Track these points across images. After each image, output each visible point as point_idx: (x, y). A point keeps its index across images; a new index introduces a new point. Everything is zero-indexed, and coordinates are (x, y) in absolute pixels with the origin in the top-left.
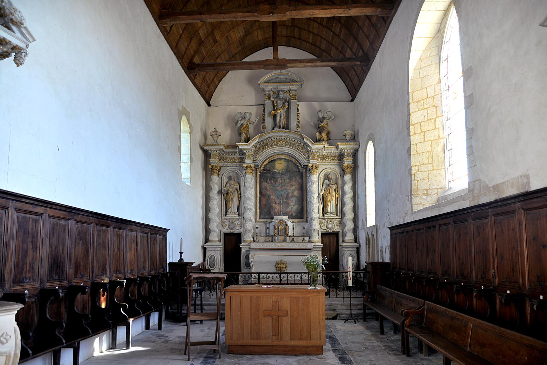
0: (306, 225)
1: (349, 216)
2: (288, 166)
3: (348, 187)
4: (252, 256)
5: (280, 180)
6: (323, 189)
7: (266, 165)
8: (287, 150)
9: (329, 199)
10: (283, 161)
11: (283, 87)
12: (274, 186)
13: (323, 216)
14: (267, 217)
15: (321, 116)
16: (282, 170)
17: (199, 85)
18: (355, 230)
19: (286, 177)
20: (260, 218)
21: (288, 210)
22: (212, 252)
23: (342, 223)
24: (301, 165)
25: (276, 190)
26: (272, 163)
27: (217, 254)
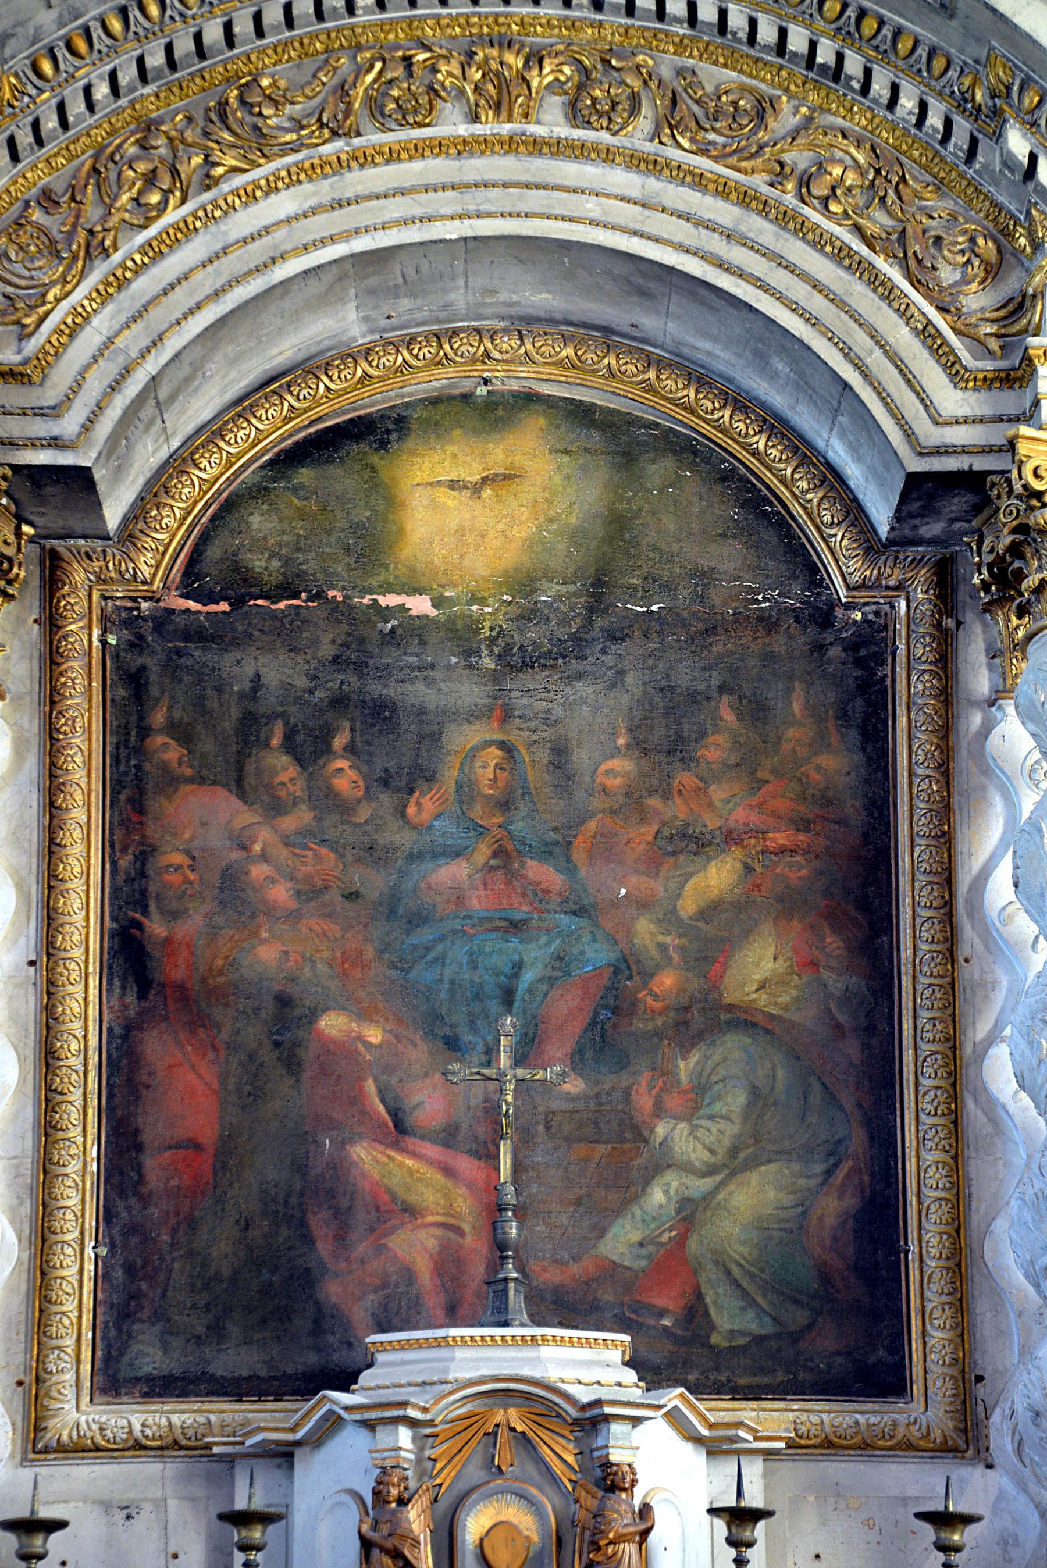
2: (618, 526)
5: (472, 751)
7: (229, 508)
8: (612, 200)
12: (373, 853)
14: (235, 1359)
16: (523, 584)
19: (594, 716)
20: (112, 1381)
21: (622, 1241)
25: (402, 913)
26: (340, 478)
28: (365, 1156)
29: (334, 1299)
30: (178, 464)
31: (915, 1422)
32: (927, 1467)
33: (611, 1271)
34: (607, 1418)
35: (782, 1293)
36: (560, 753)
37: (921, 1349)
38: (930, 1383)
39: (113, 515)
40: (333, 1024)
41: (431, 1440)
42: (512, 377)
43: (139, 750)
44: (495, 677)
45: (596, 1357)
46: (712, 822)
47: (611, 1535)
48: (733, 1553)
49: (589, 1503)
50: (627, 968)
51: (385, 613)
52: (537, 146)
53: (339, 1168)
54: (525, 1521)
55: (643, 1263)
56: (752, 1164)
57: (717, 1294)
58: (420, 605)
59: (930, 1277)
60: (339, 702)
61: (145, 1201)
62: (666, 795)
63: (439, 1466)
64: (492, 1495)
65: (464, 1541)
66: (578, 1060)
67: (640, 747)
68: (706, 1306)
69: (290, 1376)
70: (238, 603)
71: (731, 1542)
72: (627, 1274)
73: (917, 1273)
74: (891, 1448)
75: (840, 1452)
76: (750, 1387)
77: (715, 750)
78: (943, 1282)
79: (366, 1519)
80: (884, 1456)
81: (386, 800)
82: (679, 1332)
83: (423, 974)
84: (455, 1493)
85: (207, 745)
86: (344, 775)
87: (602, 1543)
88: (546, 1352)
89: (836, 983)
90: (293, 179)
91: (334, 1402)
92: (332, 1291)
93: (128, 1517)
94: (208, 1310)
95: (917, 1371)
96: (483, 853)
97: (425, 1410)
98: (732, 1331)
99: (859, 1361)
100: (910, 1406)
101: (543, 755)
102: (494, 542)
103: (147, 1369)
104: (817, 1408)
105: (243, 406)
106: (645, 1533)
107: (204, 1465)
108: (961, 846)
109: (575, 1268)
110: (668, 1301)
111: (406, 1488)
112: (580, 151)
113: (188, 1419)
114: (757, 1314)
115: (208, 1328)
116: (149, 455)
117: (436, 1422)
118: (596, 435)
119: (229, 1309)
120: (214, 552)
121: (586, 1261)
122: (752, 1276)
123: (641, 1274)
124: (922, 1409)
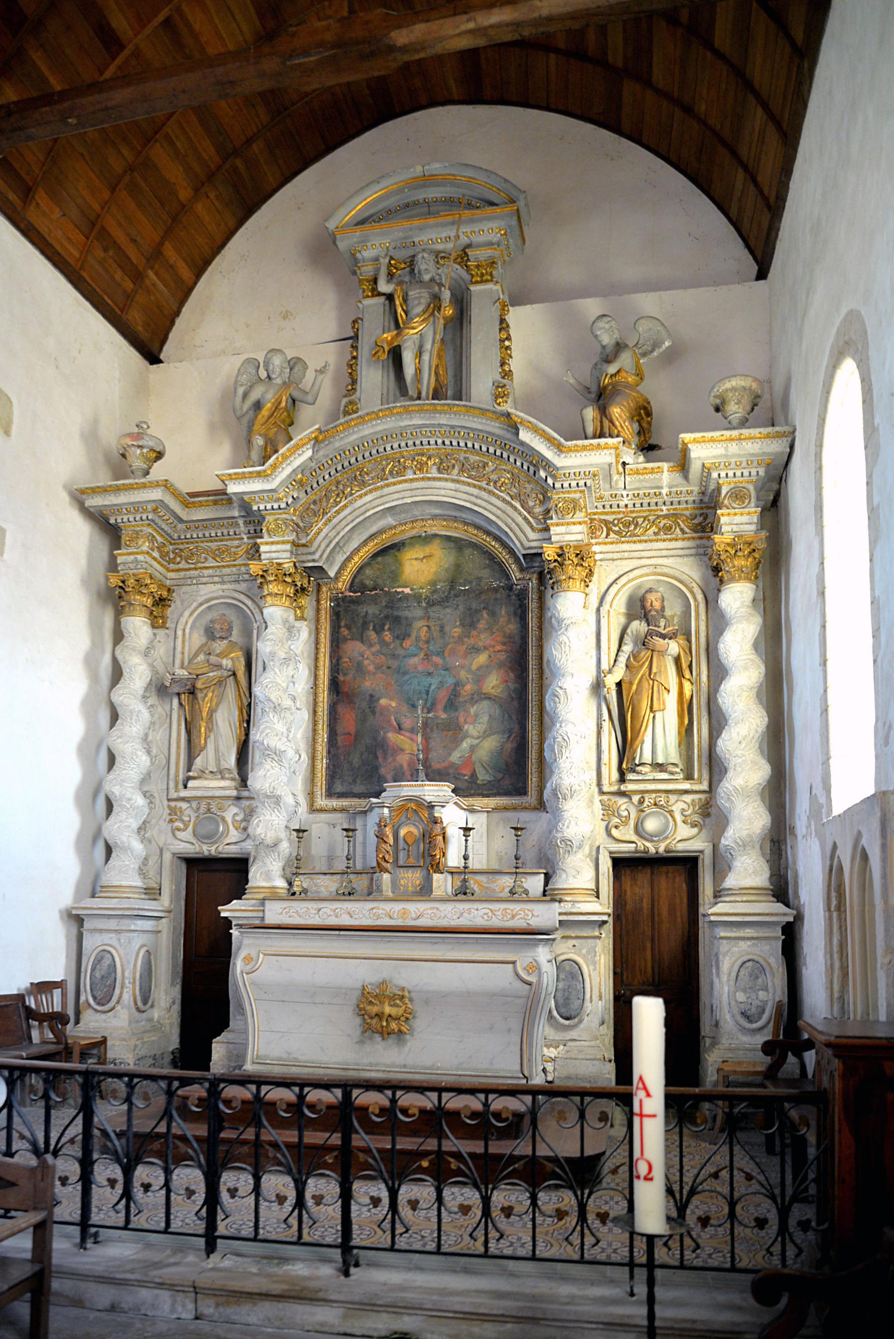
0: (536, 823)
1: (746, 771)
2: (458, 566)
3: (739, 643)
4: (248, 959)
5: (420, 628)
6: (623, 659)
7: (361, 569)
8: (449, 490)
9: (645, 704)
10: (435, 549)
11: (437, 235)
13: (622, 779)
14: (358, 788)
15: (607, 339)
16: (433, 583)
17: (72, 253)
18: (778, 843)
19: (451, 617)
20: (330, 794)
22: (107, 938)
23: (710, 813)
24: (512, 552)
25: (401, 672)
26: (388, 559)
27: (143, 942)
28: (392, 736)
30: (349, 559)
33: (452, 765)
36: (442, 627)
39: (332, 574)
40: (383, 702)
42: (435, 530)
43: (338, 632)
44: (426, 608)
46: (481, 644)
50: (457, 684)
51: (399, 593)
52: (429, 479)
53: (384, 739)
56: (489, 736)
58: (407, 590)
60: (387, 617)
61: (338, 748)
62: (469, 637)
66: (445, 709)
67: (462, 625)
70: (362, 593)
77: (482, 625)
81: (397, 642)
83: (406, 688)
85: (354, 630)
86: (387, 636)
89: (512, 686)
90: (371, 491)
92: (383, 771)
96: (422, 655)
101: (438, 628)
102: (426, 572)
105: (365, 543)
108: (545, 648)
112: (440, 479)
116: (340, 559)
118: (452, 544)
120: (357, 580)
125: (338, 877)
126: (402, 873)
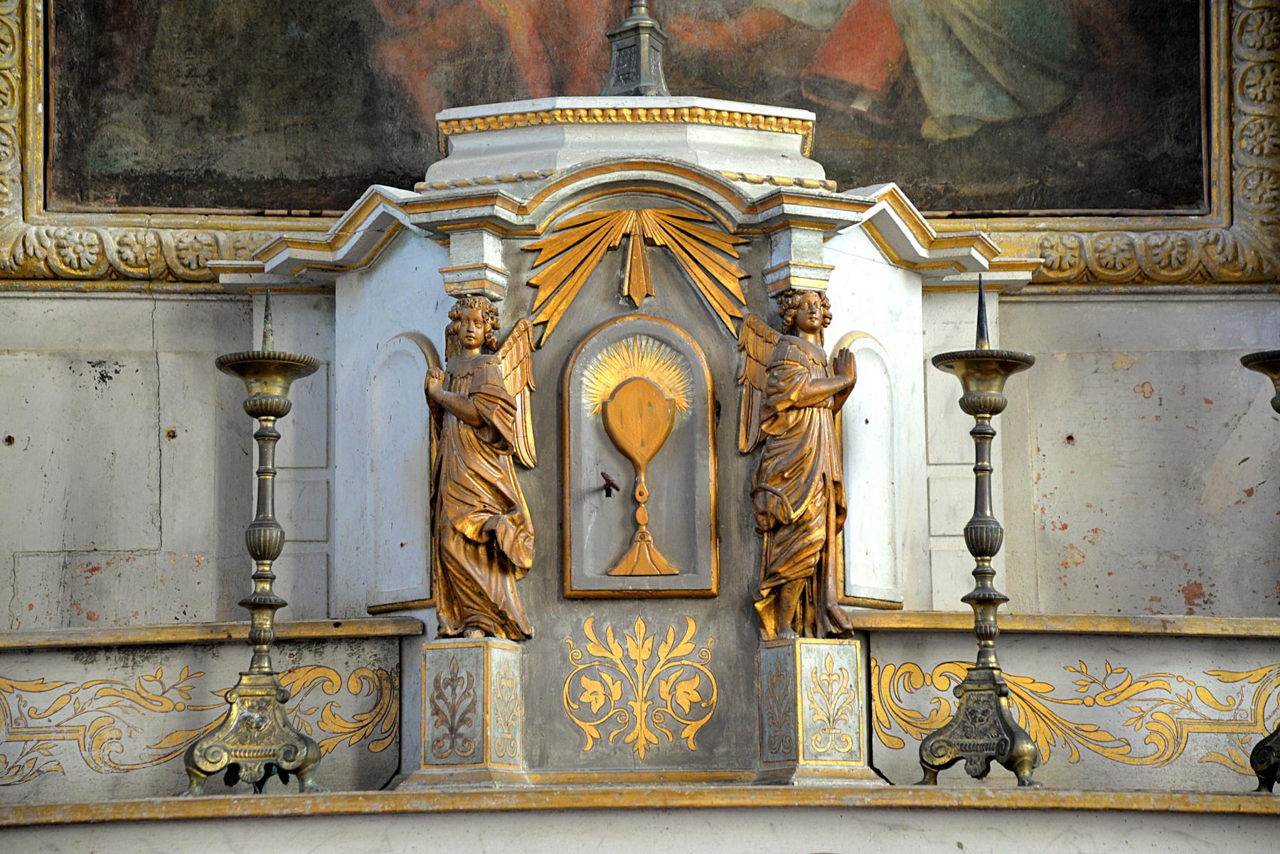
14: (254, 153)
29: (392, 70)
31: (1216, 241)
32: (1229, 307)
34: (788, 223)
35: (1025, 60)
37: (1225, 133)
38: (1238, 183)
41: (531, 257)
45: (766, 145)
47: (794, 396)
48: (970, 421)
49: (759, 352)
54: (666, 377)
55: (828, 19)
57: (932, 62)
59: (1245, 23)
63: (542, 295)
64: (620, 339)
65: (579, 405)
68: (916, 81)
69: (332, 181)
71: (970, 406)
72: (806, 35)
73: (1223, 20)
74: (1179, 281)
75: (1105, 289)
76: (977, 199)
78: (1263, 30)
79: (436, 372)
80: (1169, 293)
82: (878, 120)
84: (565, 336)
87: (781, 407)
88: (698, 135)
91: (389, 202)
92: (391, 57)
93: (103, 377)
94: (213, 79)
95: (1219, 167)
97: (522, 210)
98: (952, 117)
99: (1134, 155)
100: (1207, 219)
103: (128, 163)
104: (1072, 225)
106: (844, 393)
107: (210, 307)
109: (731, 28)
110: (863, 74)
111: (494, 327)
113: (187, 237)
114: (989, 91)
115: (213, 106)
117: (539, 230)
119: (243, 79)
121: (748, 17)
122: (982, 34)
123: (825, 36)
124: (1225, 223)
125: (173, 668)
126: (596, 639)
